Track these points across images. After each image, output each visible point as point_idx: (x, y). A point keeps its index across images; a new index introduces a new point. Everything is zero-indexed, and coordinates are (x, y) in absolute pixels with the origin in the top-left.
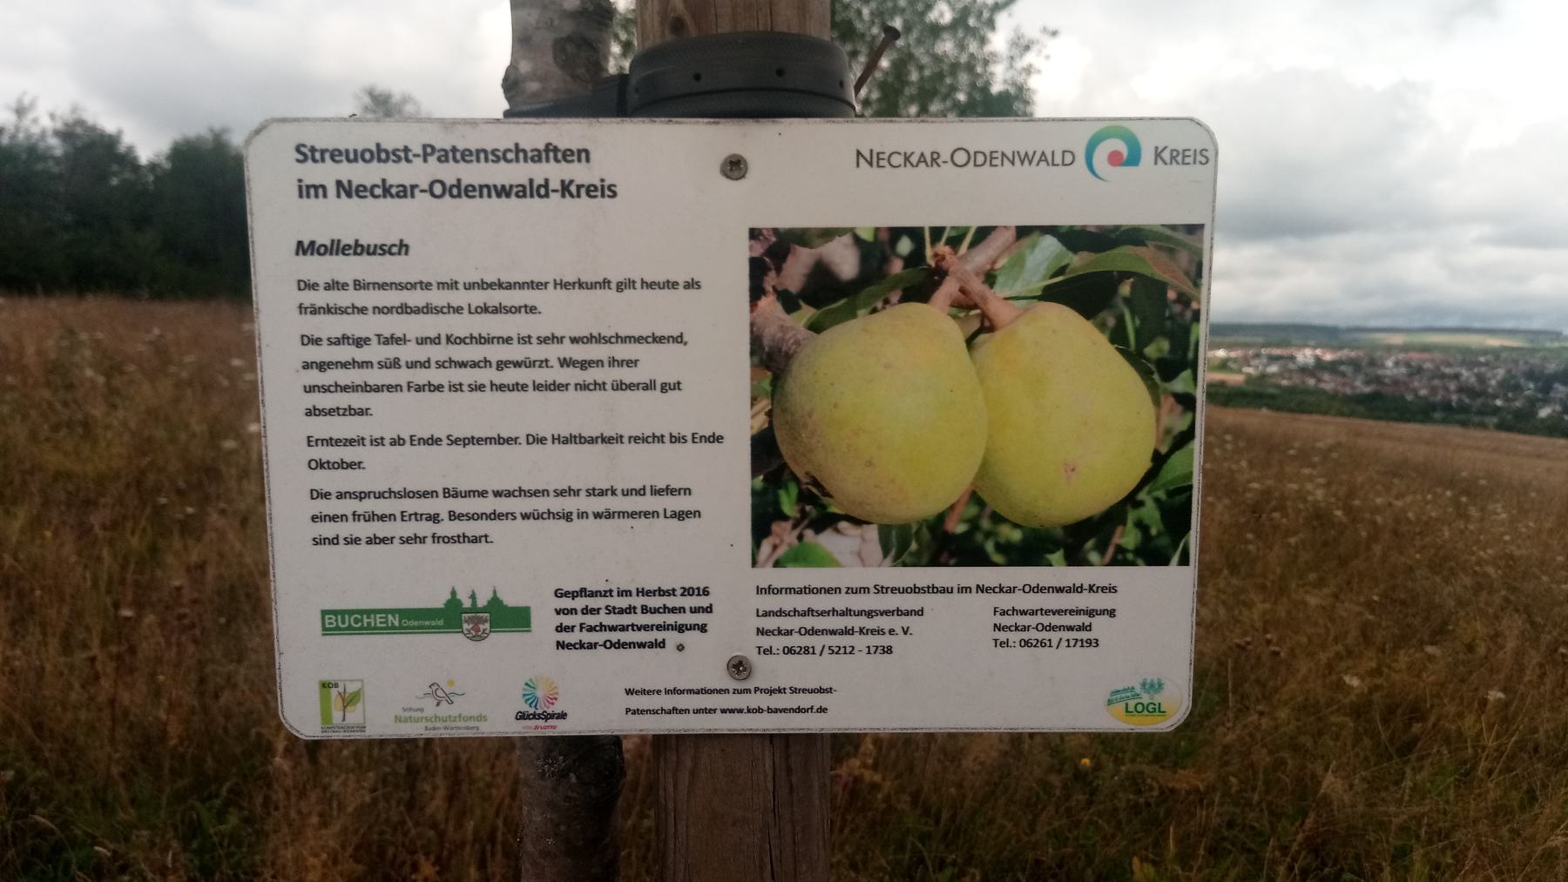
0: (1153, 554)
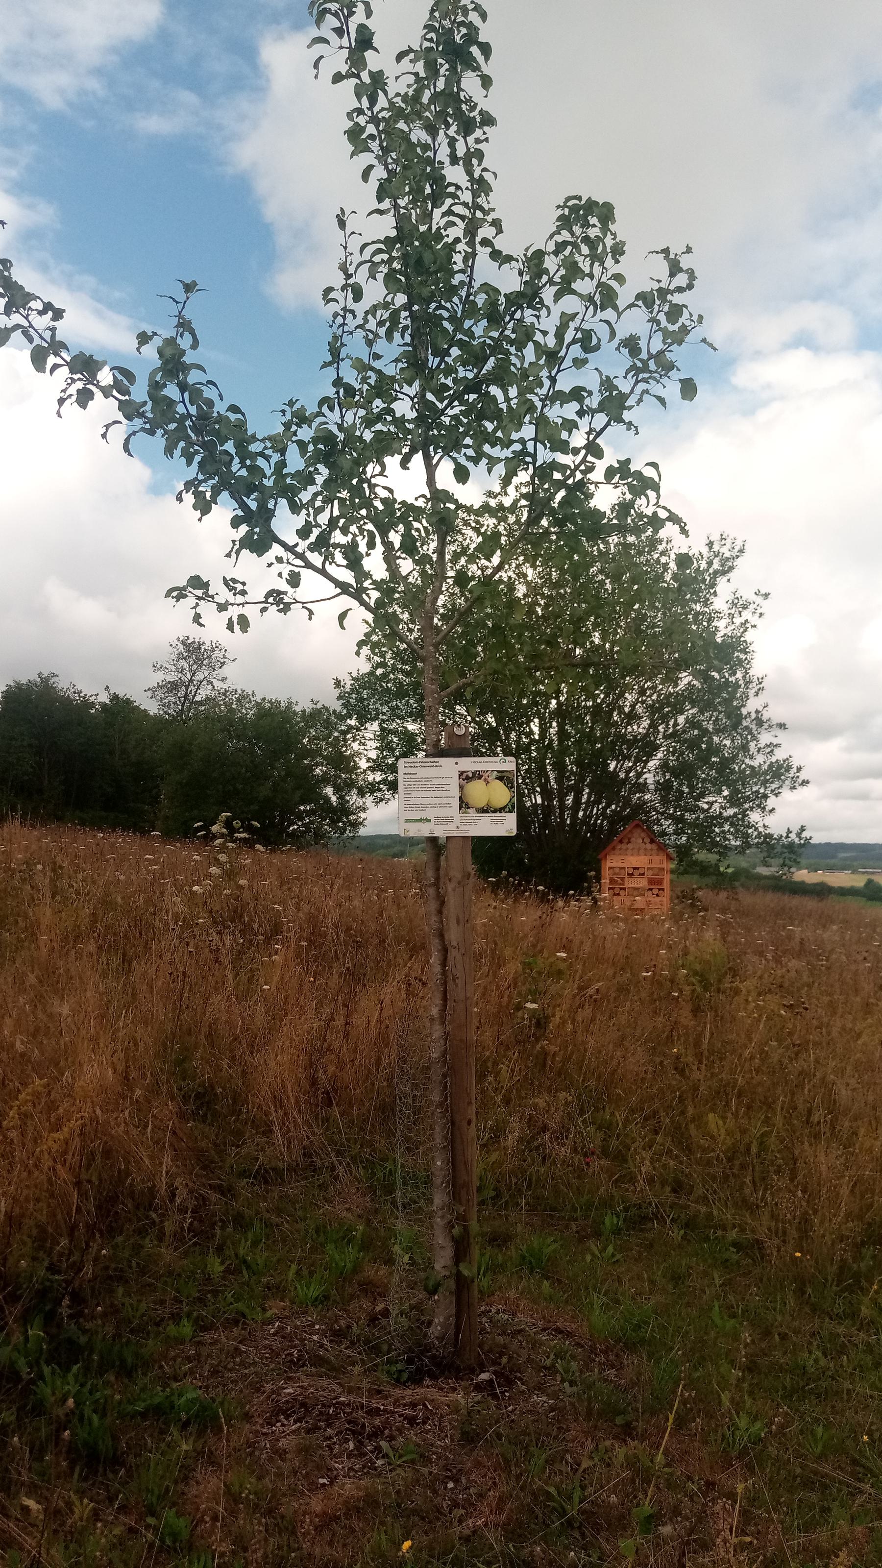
0: (510, 812)
